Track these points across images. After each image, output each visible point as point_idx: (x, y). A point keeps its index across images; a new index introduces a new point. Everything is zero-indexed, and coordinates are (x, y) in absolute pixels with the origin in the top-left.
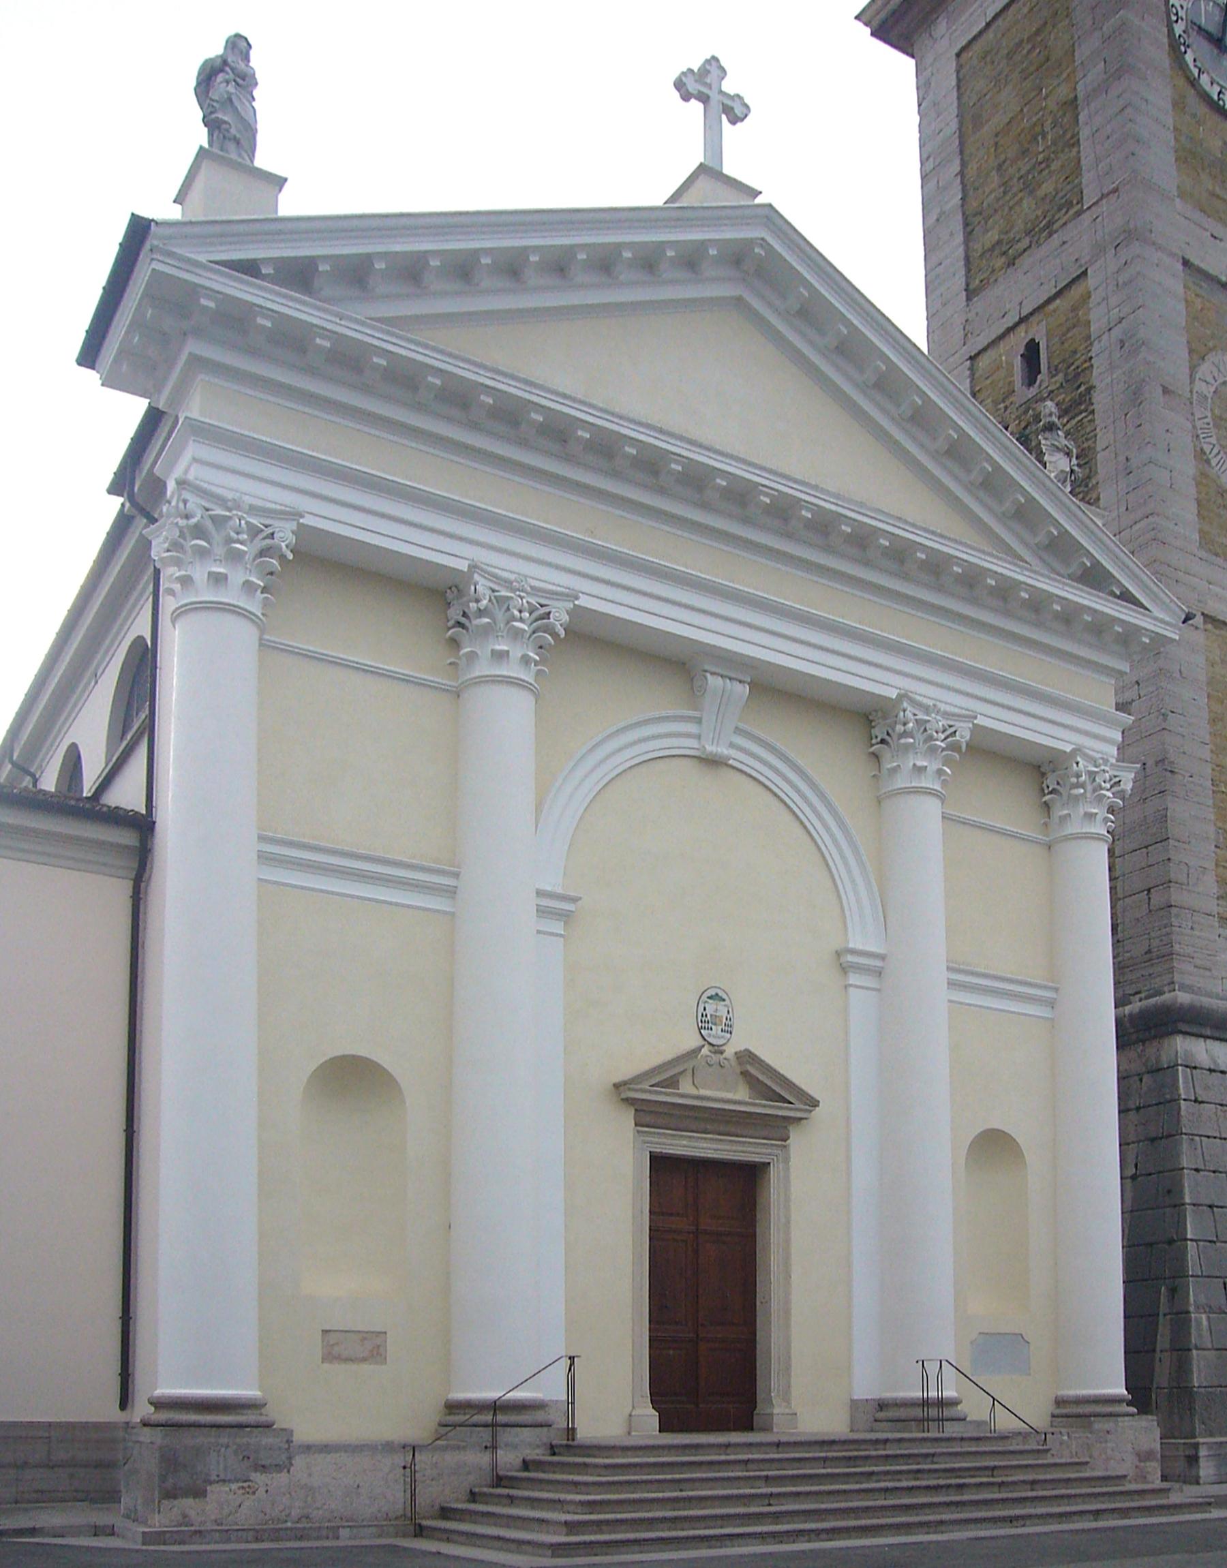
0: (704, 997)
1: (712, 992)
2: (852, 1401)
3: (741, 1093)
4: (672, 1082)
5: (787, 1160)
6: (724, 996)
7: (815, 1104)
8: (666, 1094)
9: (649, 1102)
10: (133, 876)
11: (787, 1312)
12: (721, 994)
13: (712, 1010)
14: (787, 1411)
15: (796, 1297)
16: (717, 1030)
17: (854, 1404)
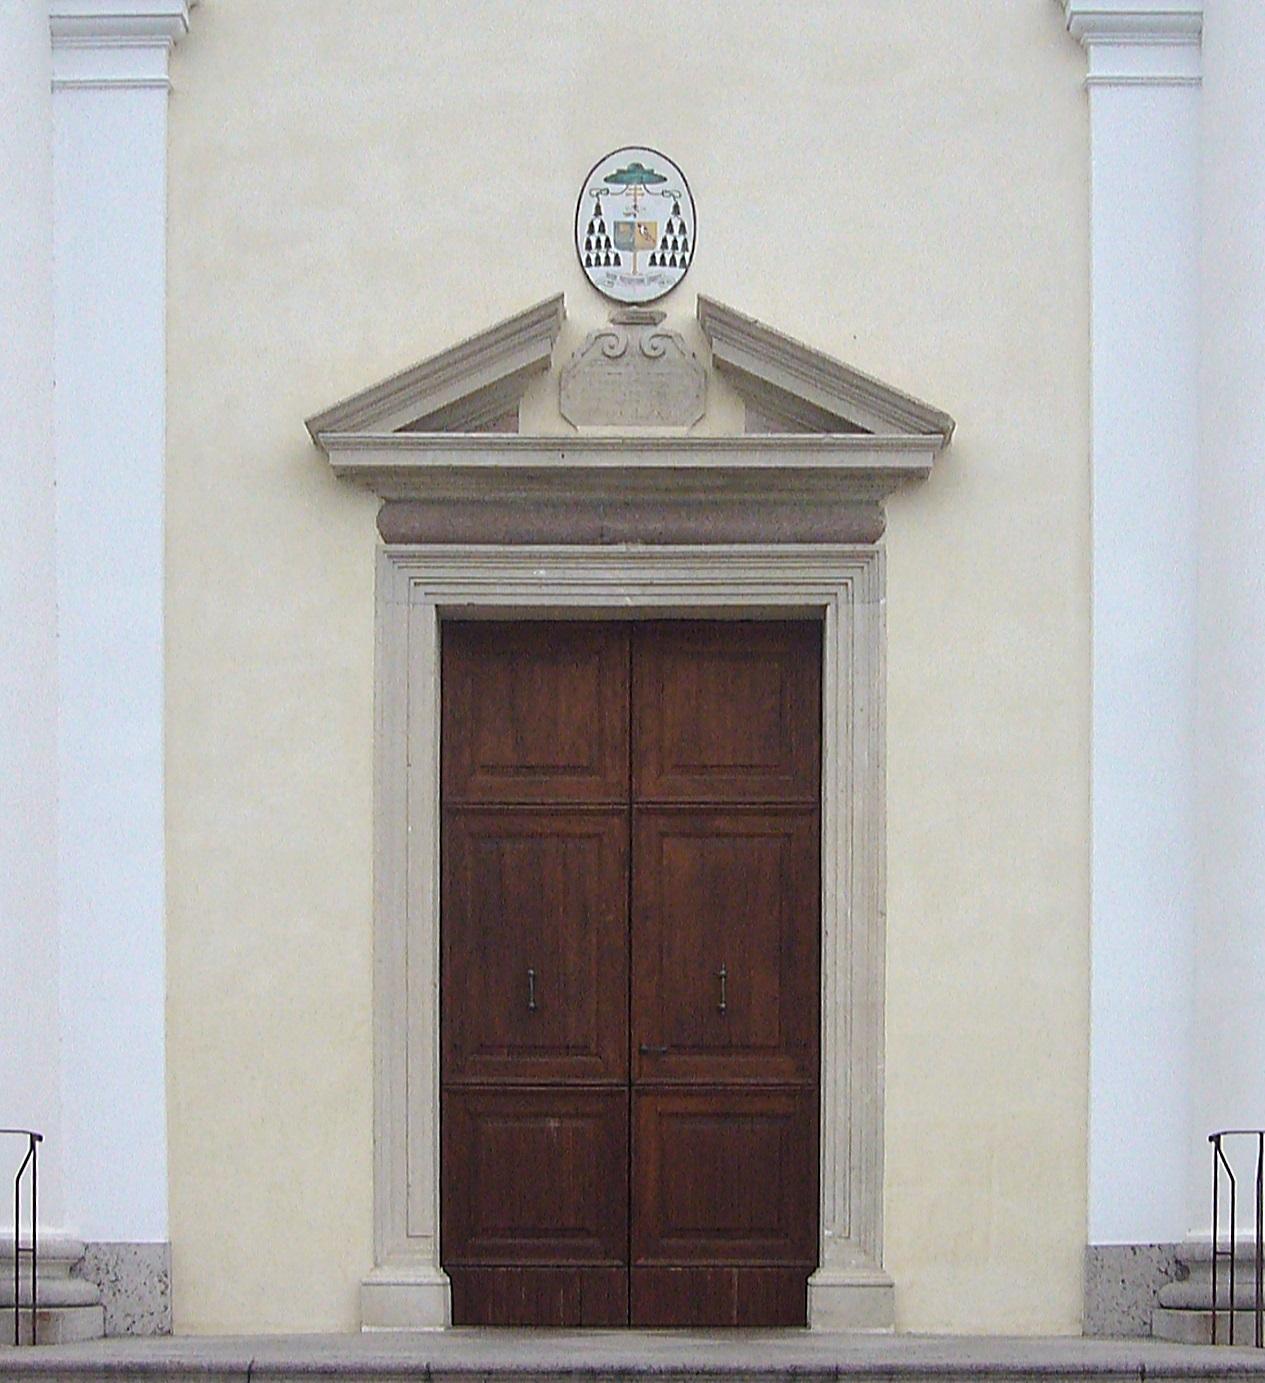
0: (598, 180)
1: (622, 162)
2: (1088, 1247)
3: (724, 419)
4: (492, 408)
5: (874, 595)
6: (661, 168)
7: (935, 427)
8: (491, 446)
9: (427, 460)
10: (449, 452)
11: (873, 1011)
12: (648, 162)
13: (632, 205)
14: (862, 1277)
15: (897, 969)
16: (635, 262)
17: (1096, 1259)
